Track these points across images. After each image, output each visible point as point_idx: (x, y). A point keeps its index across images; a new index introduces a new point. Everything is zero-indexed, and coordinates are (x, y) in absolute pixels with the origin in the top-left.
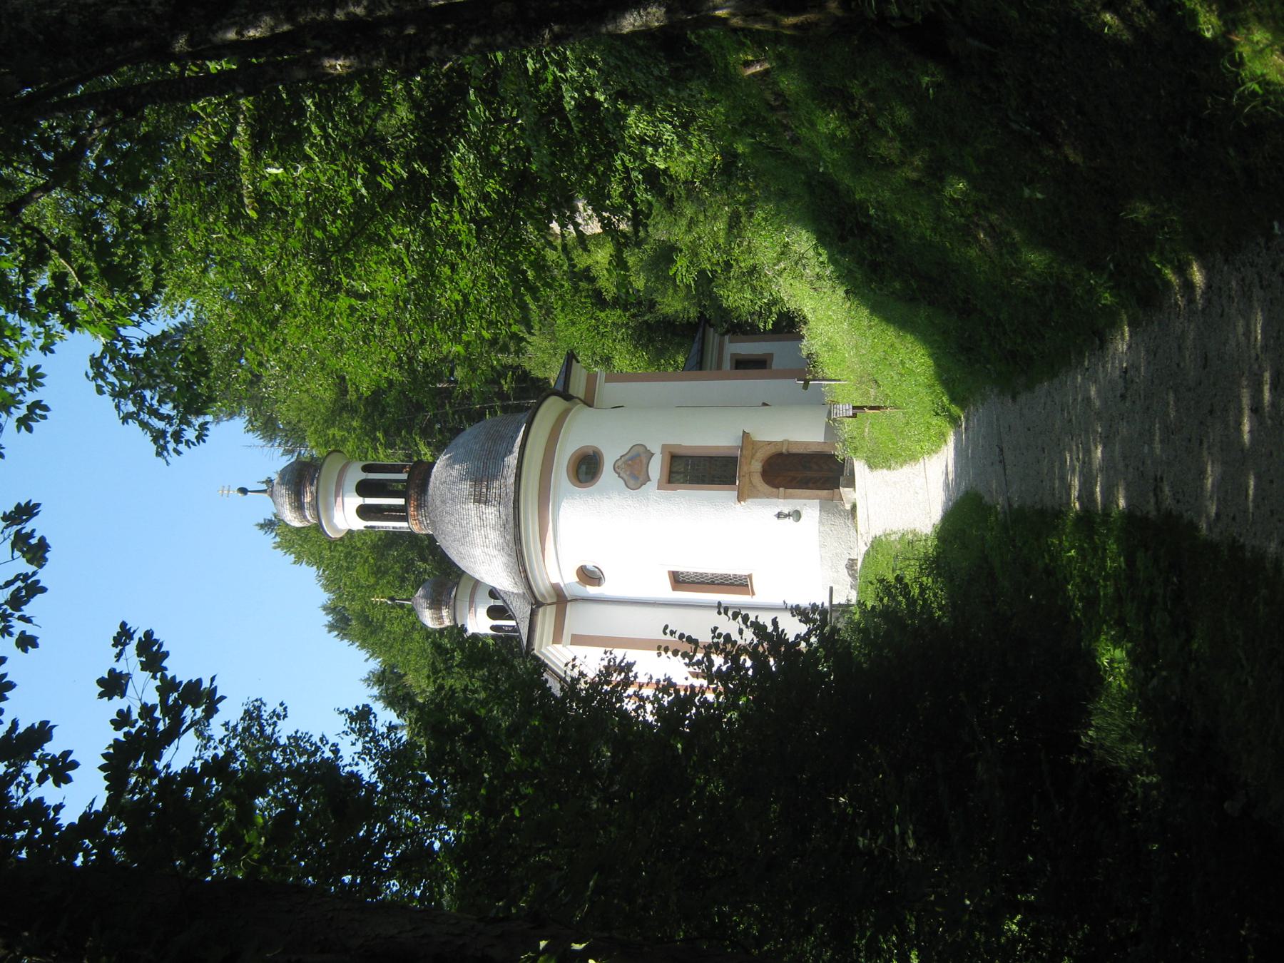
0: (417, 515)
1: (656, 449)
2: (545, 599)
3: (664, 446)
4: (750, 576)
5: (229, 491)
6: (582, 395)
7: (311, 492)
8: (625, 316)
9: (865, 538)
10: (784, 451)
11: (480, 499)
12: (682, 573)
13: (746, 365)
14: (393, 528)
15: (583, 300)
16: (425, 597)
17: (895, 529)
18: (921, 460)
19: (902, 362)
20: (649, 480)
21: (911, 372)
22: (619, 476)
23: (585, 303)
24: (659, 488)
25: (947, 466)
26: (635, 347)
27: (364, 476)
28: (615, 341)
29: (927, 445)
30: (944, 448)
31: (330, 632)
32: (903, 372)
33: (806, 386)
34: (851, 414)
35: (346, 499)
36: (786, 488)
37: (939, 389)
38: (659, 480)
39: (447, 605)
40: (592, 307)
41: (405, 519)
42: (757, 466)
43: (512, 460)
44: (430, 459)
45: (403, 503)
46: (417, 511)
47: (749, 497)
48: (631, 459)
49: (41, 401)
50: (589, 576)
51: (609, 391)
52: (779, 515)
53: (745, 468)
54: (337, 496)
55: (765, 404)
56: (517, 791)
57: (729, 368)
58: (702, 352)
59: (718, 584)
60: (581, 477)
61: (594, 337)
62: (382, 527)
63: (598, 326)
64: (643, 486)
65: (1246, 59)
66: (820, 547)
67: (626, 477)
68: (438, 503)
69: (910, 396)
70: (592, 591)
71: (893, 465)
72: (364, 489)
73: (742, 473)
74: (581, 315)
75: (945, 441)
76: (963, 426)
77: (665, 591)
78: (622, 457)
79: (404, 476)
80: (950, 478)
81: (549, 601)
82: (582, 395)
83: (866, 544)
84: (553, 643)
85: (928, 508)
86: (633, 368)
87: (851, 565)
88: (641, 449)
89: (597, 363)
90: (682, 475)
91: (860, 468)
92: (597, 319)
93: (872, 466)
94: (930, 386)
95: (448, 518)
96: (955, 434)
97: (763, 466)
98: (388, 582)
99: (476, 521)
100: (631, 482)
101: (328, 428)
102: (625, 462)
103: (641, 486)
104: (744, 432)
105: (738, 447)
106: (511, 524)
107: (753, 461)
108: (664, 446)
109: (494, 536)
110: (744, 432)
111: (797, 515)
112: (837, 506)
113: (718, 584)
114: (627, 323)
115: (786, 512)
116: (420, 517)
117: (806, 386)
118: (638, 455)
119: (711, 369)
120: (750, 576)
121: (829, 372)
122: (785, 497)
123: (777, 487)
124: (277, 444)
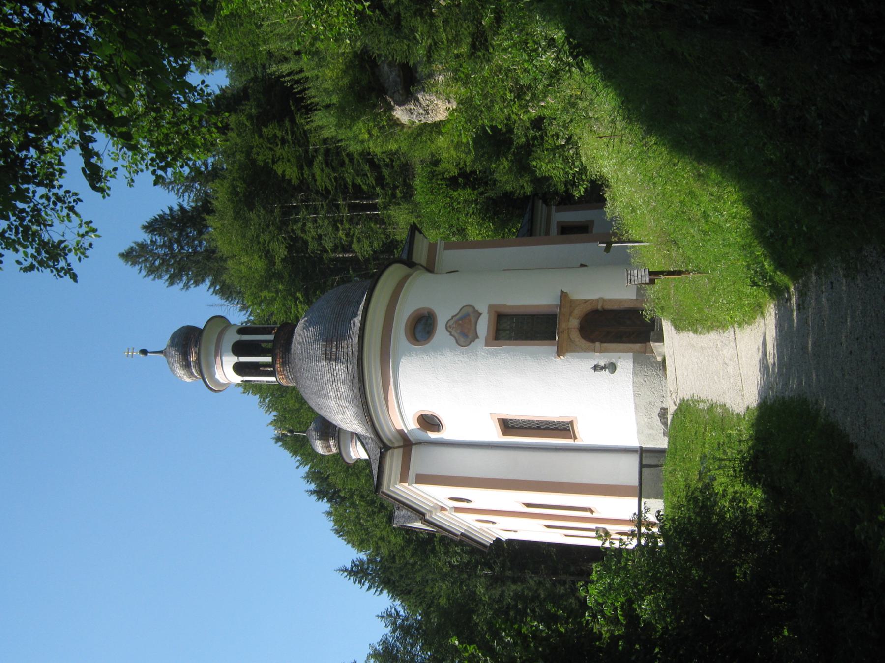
0: (283, 371)
1: (483, 309)
2: (393, 443)
3: (491, 307)
4: (571, 423)
5: (133, 352)
6: (424, 262)
7: (196, 353)
8: (474, 194)
9: (674, 396)
10: (599, 308)
11: (331, 358)
12: (511, 420)
13: (569, 231)
14: (266, 381)
15: (439, 182)
16: (316, 430)
17: (703, 397)
18: (731, 330)
19: (705, 215)
20: (477, 337)
21: (718, 228)
22: (451, 335)
23: (442, 184)
24: (487, 344)
25: (764, 344)
26: (483, 219)
27: (238, 338)
28: (467, 214)
29: (738, 316)
30: (759, 321)
31: (276, 442)
32: (707, 228)
33: (608, 249)
34: (647, 281)
35: (224, 358)
36: (602, 342)
37: (759, 251)
38: (486, 337)
39: (333, 437)
40: (447, 188)
41: (272, 374)
42: (575, 323)
43: (356, 322)
44: (295, 323)
45: (271, 361)
46: (283, 367)
47: (568, 351)
48: (462, 319)
50: (429, 422)
51: (448, 257)
52: (596, 368)
53: (564, 325)
54: (216, 356)
55: (582, 265)
58: (532, 221)
59: (544, 429)
60: (418, 336)
61: (450, 212)
62: (258, 381)
63: (452, 203)
64: (472, 343)
66: (635, 396)
67: (456, 335)
68: (297, 360)
69: (717, 261)
70: (433, 435)
71: (700, 329)
72: (239, 349)
73: (561, 330)
74: (439, 195)
75: (762, 313)
76: (794, 300)
77: (494, 435)
78: (453, 317)
79: (271, 337)
80: (771, 361)
81: (396, 445)
82: (424, 262)
83: (674, 403)
84: (400, 482)
85: (739, 383)
86: (482, 237)
87: (663, 413)
88: (470, 310)
89: (454, 234)
90: (508, 332)
91: (667, 327)
92: (451, 198)
93: (678, 328)
94: (744, 247)
95: (306, 374)
96: (778, 307)
97: (581, 323)
99: (328, 376)
100: (462, 340)
101: (261, 291)
102: (456, 322)
103: (470, 343)
104: (562, 292)
105: (556, 306)
106: (356, 380)
107: (571, 318)
108: (491, 307)
109: (344, 389)
110: (562, 292)
111: (612, 367)
112: (649, 358)
113: (544, 429)
114: (476, 200)
115: (603, 365)
116: (285, 372)
117: (608, 249)
118: (468, 315)
119: (540, 235)
120: (571, 423)
121: (634, 233)
122: (601, 351)
123: (593, 341)
124: (235, 303)
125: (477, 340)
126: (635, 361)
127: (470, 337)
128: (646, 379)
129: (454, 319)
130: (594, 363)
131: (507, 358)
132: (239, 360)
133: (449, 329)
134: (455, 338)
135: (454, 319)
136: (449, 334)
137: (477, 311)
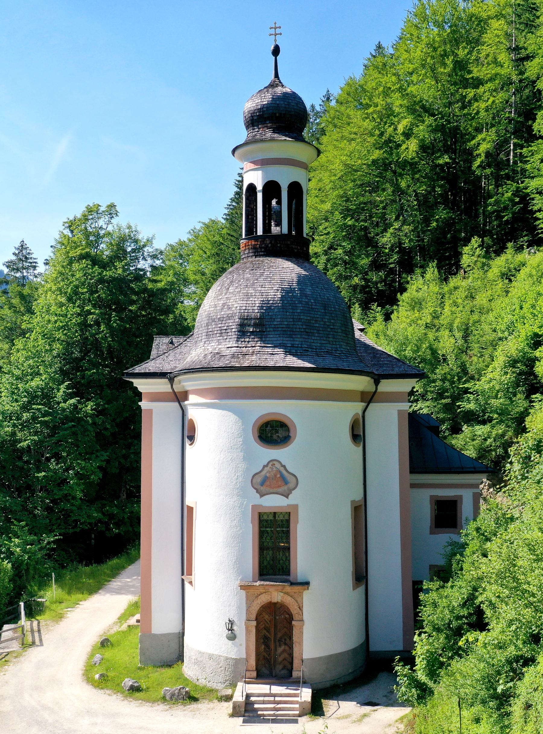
1: (294, 498)
22: (264, 466)
48: (283, 477)
52: (231, 622)
54: (254, 162)
66: (210, 655)
67: (263, 473)
78: (284, 467)
88: (291, 485)
100: (259, 479)
103: (255, 489)
108: (296, 507)
111: (232, 637)
118: (286, 482)
125: (258, 495)
126: (237, 661)
127: (262, 488)
128: (222, 668)
129: (282, 469)
130: (236, 620)
131: (241, 529)
132: (259, 191)
133: (271, 463)
134: (261, 472)
135: (282, 469)
136: (266, 464)
137: (291, 493)
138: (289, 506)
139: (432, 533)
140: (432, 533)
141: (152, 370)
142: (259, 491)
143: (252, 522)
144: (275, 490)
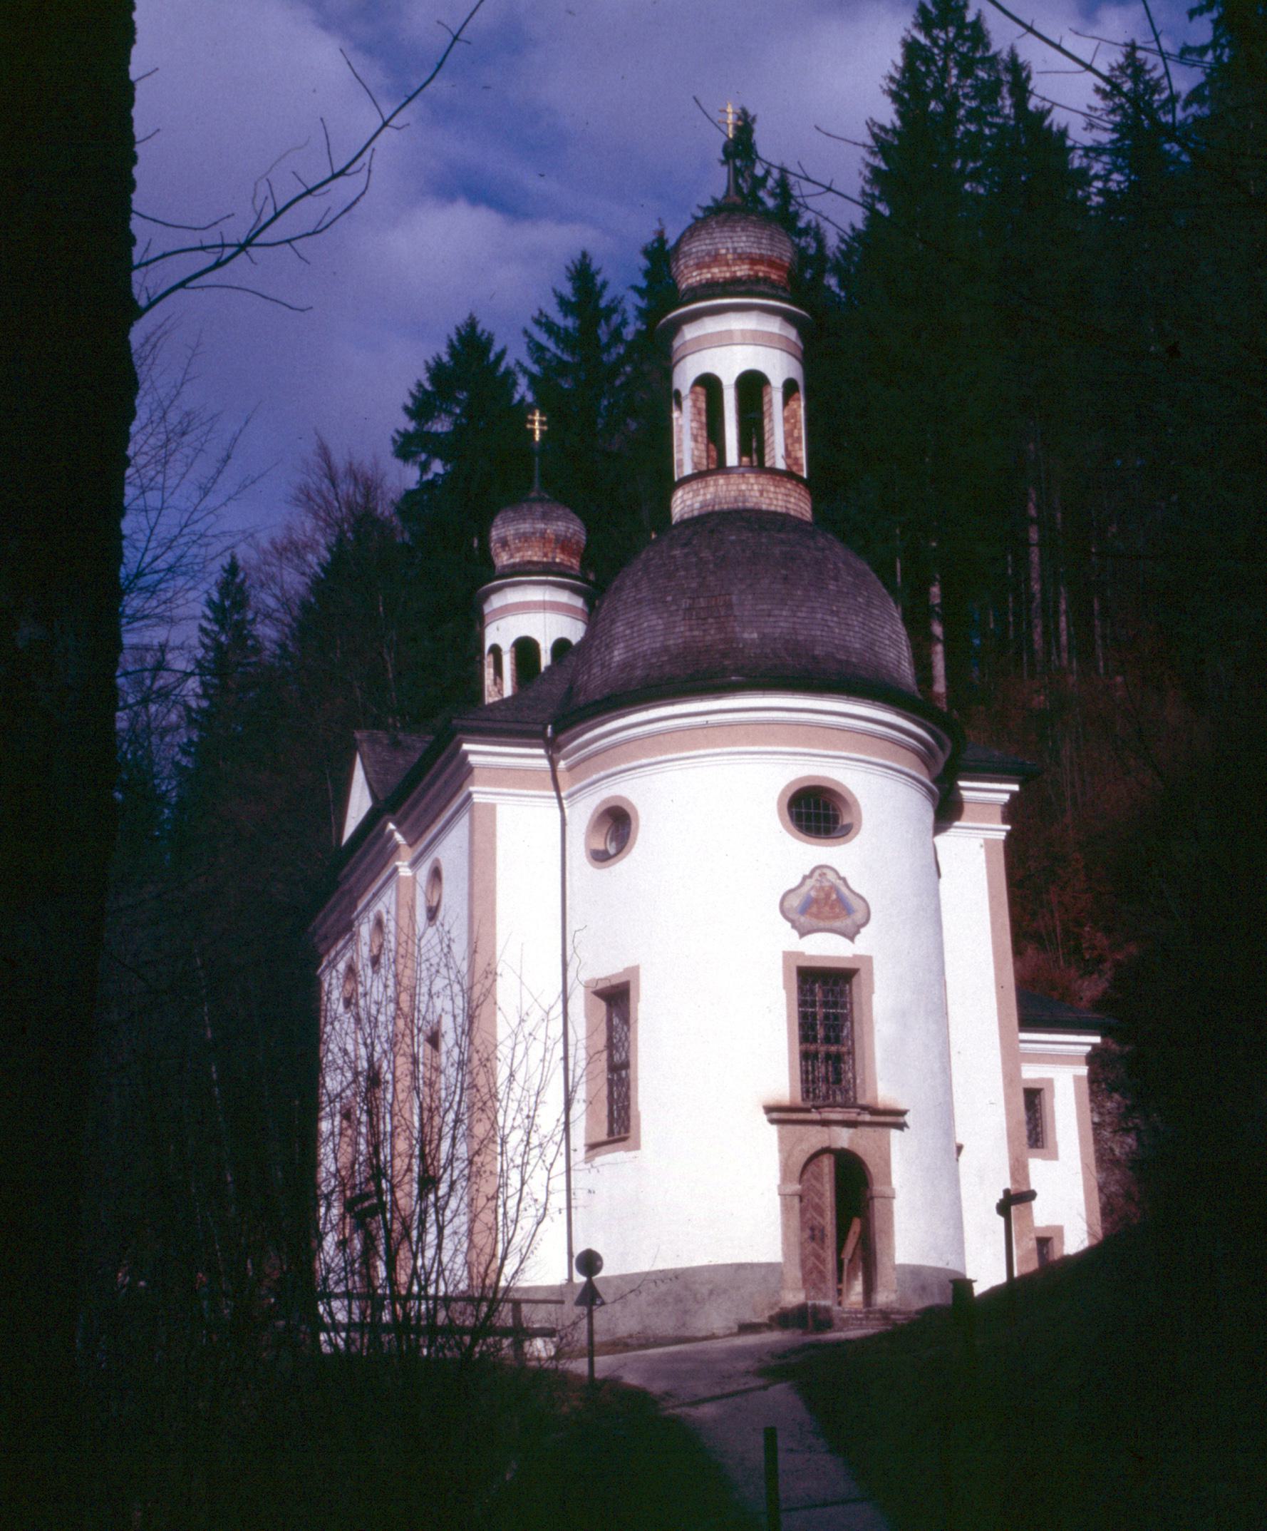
1: (863, 945)
3: (868, 960)
20: (803, 933)
22: (805, 878)
42: (842, 1138)
48: (841, 900)
49: (406, 409)
56: (1118, 186)
57: (1058, 1087)
64: (789, 925)
65: (369, 964)
78: (844, 880)
88: (859, 917)
98: (174, 702)
100: (795, 902)
102: (834, 888)
108: (868, 960)
125: (795, 934)
135: (839, 883)
136: (807, 872)
138: (856, 957)
139: (634, 971)
140: (634, 971)
141: (816, 186)
142: (797, 924)
143: (786, 987)
144: (827, 924)
